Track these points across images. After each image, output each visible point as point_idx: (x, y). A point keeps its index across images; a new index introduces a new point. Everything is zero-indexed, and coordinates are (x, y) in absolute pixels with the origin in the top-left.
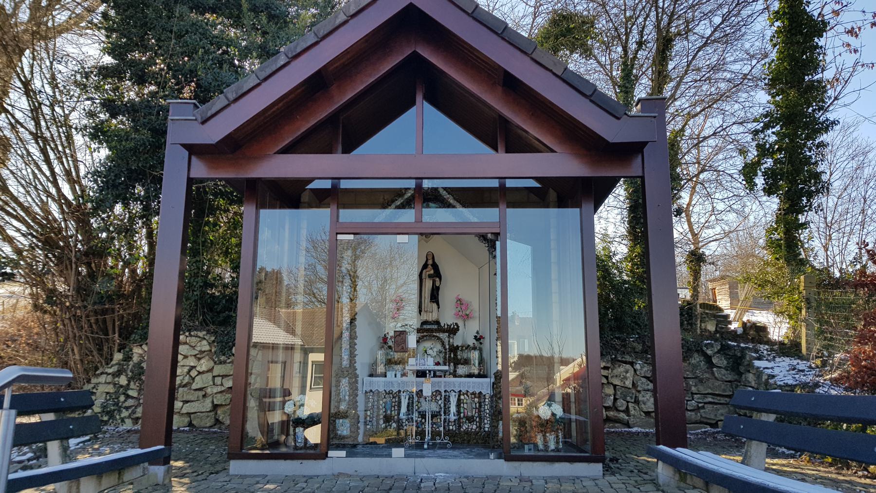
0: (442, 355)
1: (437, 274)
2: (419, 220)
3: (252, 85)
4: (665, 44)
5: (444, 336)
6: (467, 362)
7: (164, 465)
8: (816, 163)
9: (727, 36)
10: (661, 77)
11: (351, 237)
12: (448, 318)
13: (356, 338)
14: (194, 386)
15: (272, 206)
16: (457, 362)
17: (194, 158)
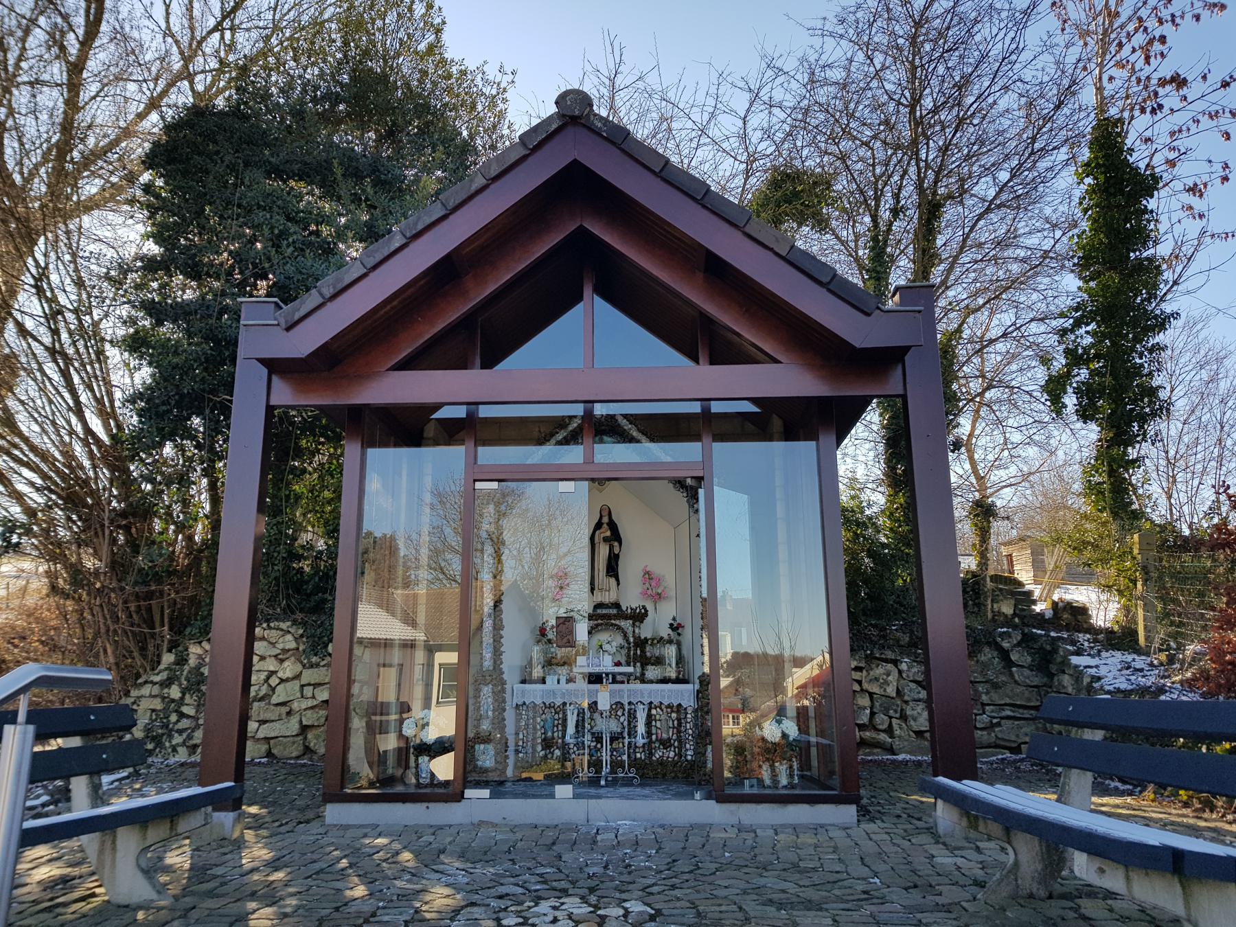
0: (624, 652)
1: (616, 536)
2: (589, 460)
4: (931, 210)
5: (626, 624)
6: (659, 661)
7: (233, 811)
9: (1017, 198)
10: (926, 257)
12: (632, 599)
13: (502, 628)
14: (275, 700)
16: (645, 662)
17: (275, 379)
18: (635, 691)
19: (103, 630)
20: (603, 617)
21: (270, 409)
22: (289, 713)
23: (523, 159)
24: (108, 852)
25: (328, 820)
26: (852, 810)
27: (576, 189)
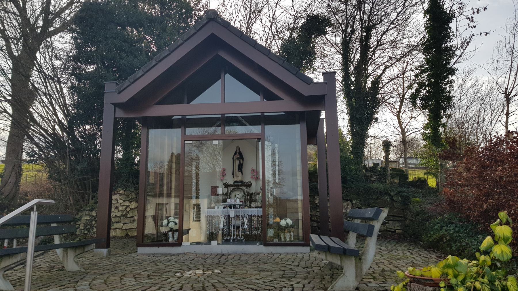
0: (244, 198)
1: (241, 157)
2: (223, 133)
3: (140, 75)
4: (368, 29)
5: (244, 188)
6: (255, 201)
7: (107, 248)
8: (449, 92)
9: (400, 24)
10: (365, 47)
11: (191, 142)
12: (247, 179)
13: (199, 190)
14: (128, 216)
15: (156, 128)
16: (251, 201)
17: (117, 109)
18: (246, 211)
19: (68, 191)
20: (236, 185)
21: (115, 118)
22: (134, 220)
23: (195, 33)
24: (65, 257)
25: (138, 252)
26: (308, 248)
27: (213, 42)
